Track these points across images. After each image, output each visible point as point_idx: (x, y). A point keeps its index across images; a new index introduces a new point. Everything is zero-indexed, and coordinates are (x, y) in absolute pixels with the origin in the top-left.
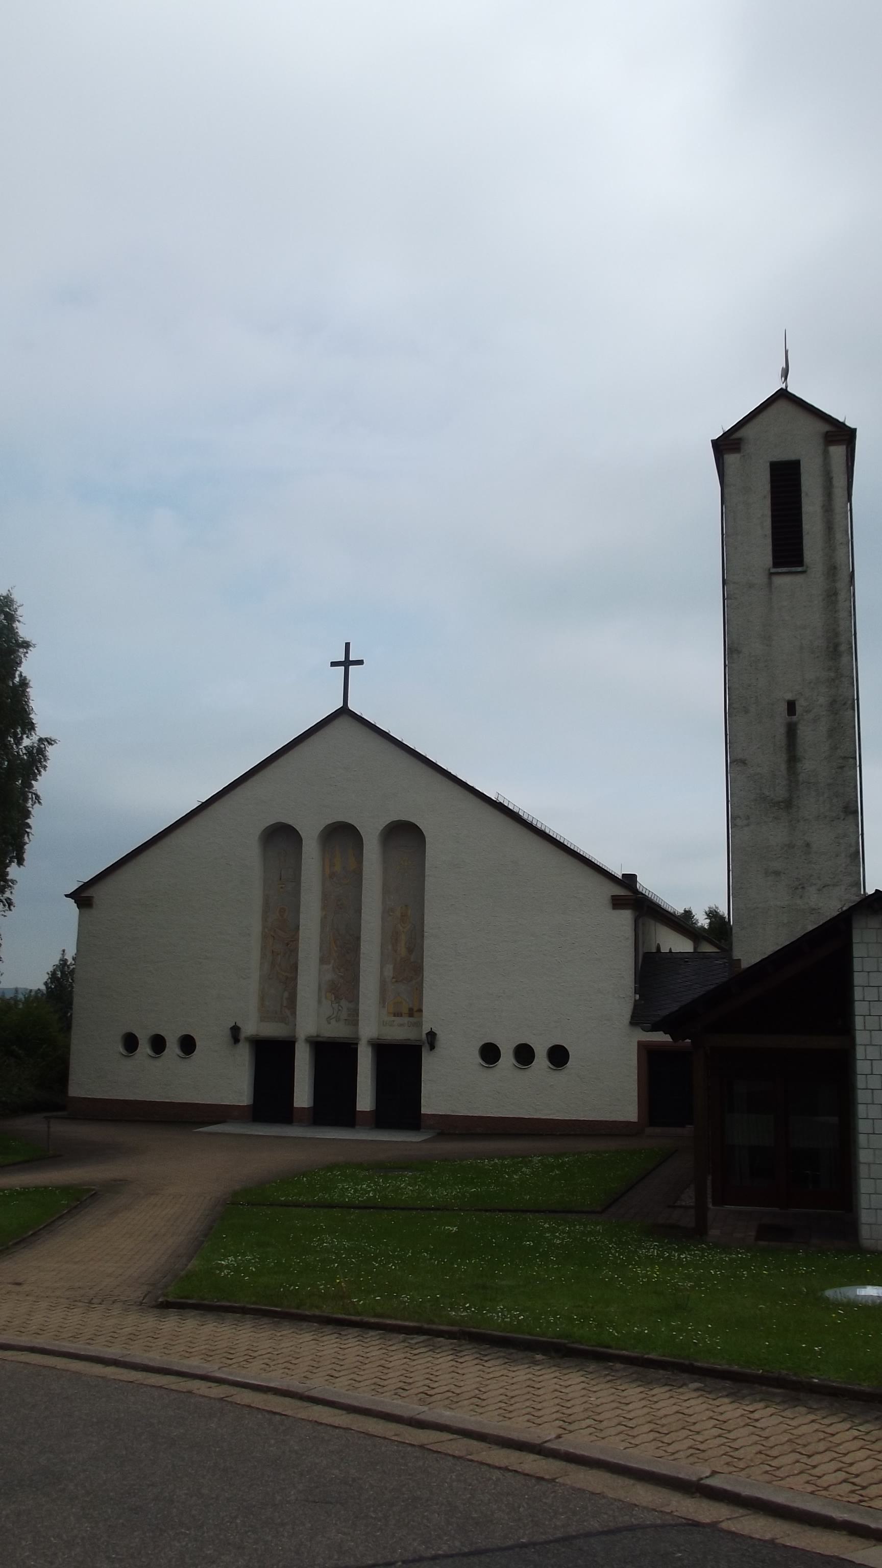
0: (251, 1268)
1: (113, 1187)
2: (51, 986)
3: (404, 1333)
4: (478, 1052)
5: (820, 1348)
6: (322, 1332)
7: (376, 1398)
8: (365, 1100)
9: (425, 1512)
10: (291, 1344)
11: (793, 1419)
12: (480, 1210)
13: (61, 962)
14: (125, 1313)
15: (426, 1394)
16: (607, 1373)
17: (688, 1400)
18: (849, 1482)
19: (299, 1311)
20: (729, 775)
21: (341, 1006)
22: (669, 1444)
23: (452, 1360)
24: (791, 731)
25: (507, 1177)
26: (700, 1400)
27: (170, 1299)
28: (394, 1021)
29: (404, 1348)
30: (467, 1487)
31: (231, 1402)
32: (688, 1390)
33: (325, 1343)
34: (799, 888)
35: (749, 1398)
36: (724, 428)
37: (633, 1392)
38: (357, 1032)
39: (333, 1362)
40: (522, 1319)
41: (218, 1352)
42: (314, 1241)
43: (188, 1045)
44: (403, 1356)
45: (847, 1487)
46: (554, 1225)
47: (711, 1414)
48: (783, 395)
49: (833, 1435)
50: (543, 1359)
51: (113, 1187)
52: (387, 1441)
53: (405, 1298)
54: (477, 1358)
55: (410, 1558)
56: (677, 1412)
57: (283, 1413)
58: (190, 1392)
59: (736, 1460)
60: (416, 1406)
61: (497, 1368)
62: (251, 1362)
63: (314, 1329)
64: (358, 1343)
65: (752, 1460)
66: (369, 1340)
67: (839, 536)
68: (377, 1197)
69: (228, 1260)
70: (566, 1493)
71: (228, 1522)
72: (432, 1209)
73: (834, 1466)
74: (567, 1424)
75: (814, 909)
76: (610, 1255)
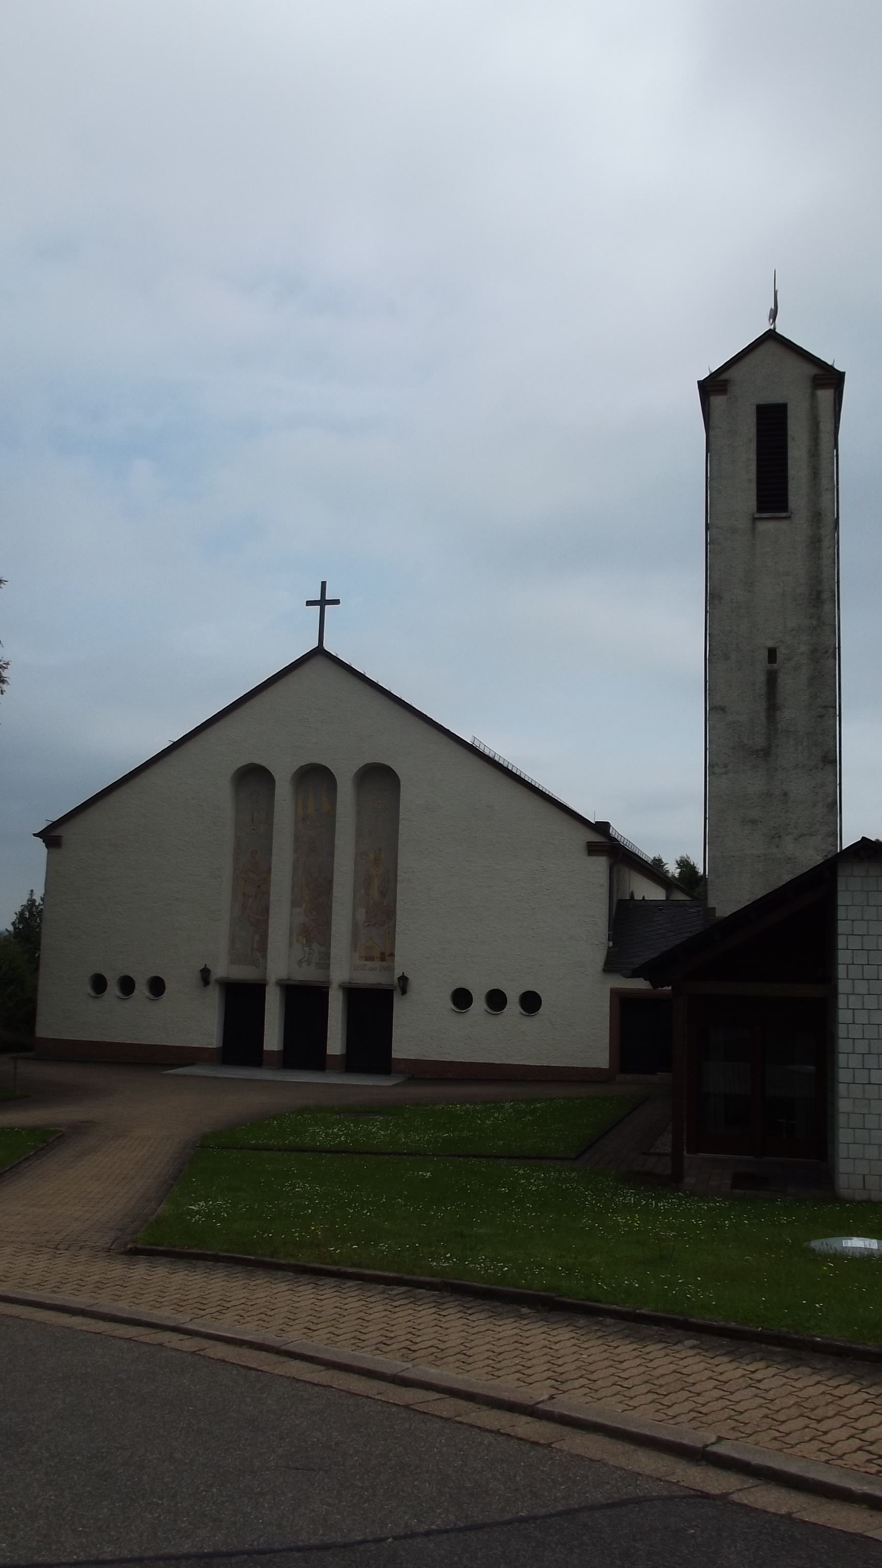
0: (222, 1214)
1: (79, 1130)
2: (19, 927)
3: (383, 1284)
5: (821, 1304)
6: (298, 1282)
7: (357, 1353)
8: (335, 1044)
9: (415, 1481)
10: (265, 1294)
11: (796, 1380)
12: (454, 1156)
13: (30, 903)
14: (93, 1260)
15: (409, 1349)
16: (597, 1328)
17: (685, 1358)
18: (863, 1450)
19: (274, 1260)
20: (708, 722)
21: (312, 950)
22: (669, 1407)
23: (434, 1313)
24: (772, 679)
25: (479, 1122)
26: (698, 1358)
27: (140, 1246)
28: (365, 965)
29: (384, 1299)
30: (458, 1453)
31: (204, 1356)
32: (683, 1348)
33: (301, 1294)
35: (748, 1356)
36: (711, 370)
37: (626, 1348)
38: (328, 976)
39: (310, 1314)
40: (506, 1270)
41: (190, 1302)
42: (286, 1186)
43: (157, 986)
44: (382, 1308)
45: (862, 1456)
46: (528, 1171)
47: (711, 1374)
48: (771, 336)
49: (841, 1398)
50: (530, 1313)
51: (79, 1130)
52: (369, 1400)
53: (383, 1246)
54: (460, 1311)
55: (402, 1533)
56: (675, 1371)
57: (259, 1368)
58: (161, 1345)
59: (742, 1424)
60: (399, 1363)
61: (482, 1322)
62: (225, 1313)
63: (289, 1278)
64: (335, 1294)
65: (758, 1426)
66: (347, 1290)
67: (825, 482)
68: (349, 1141)
69: (199, 1205)
70: (564, 1459)
71: (204, 1490)
72: (405, 1154)
73: (845, 1432)
74: (559, 1383)
75: (790, 859)
76: (587, 1203)
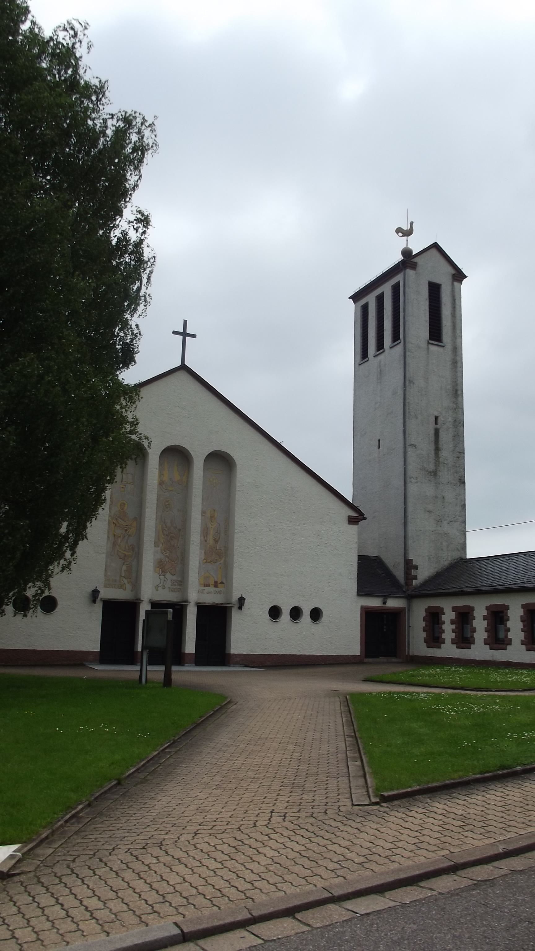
4: (58, 603)
24: (437, 432)
34: (439, 521)
67: (458, 331)
75: (446, 534)
